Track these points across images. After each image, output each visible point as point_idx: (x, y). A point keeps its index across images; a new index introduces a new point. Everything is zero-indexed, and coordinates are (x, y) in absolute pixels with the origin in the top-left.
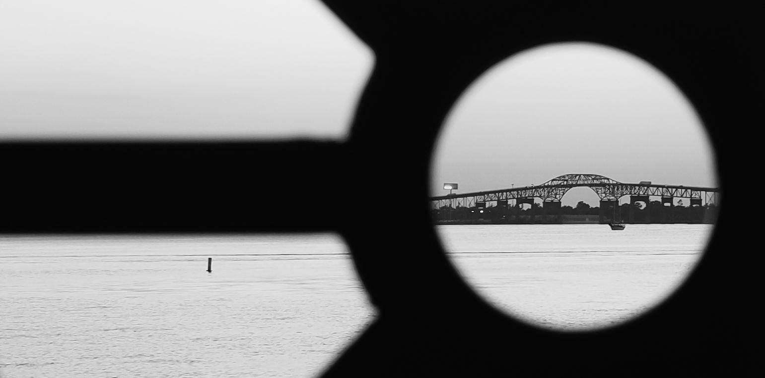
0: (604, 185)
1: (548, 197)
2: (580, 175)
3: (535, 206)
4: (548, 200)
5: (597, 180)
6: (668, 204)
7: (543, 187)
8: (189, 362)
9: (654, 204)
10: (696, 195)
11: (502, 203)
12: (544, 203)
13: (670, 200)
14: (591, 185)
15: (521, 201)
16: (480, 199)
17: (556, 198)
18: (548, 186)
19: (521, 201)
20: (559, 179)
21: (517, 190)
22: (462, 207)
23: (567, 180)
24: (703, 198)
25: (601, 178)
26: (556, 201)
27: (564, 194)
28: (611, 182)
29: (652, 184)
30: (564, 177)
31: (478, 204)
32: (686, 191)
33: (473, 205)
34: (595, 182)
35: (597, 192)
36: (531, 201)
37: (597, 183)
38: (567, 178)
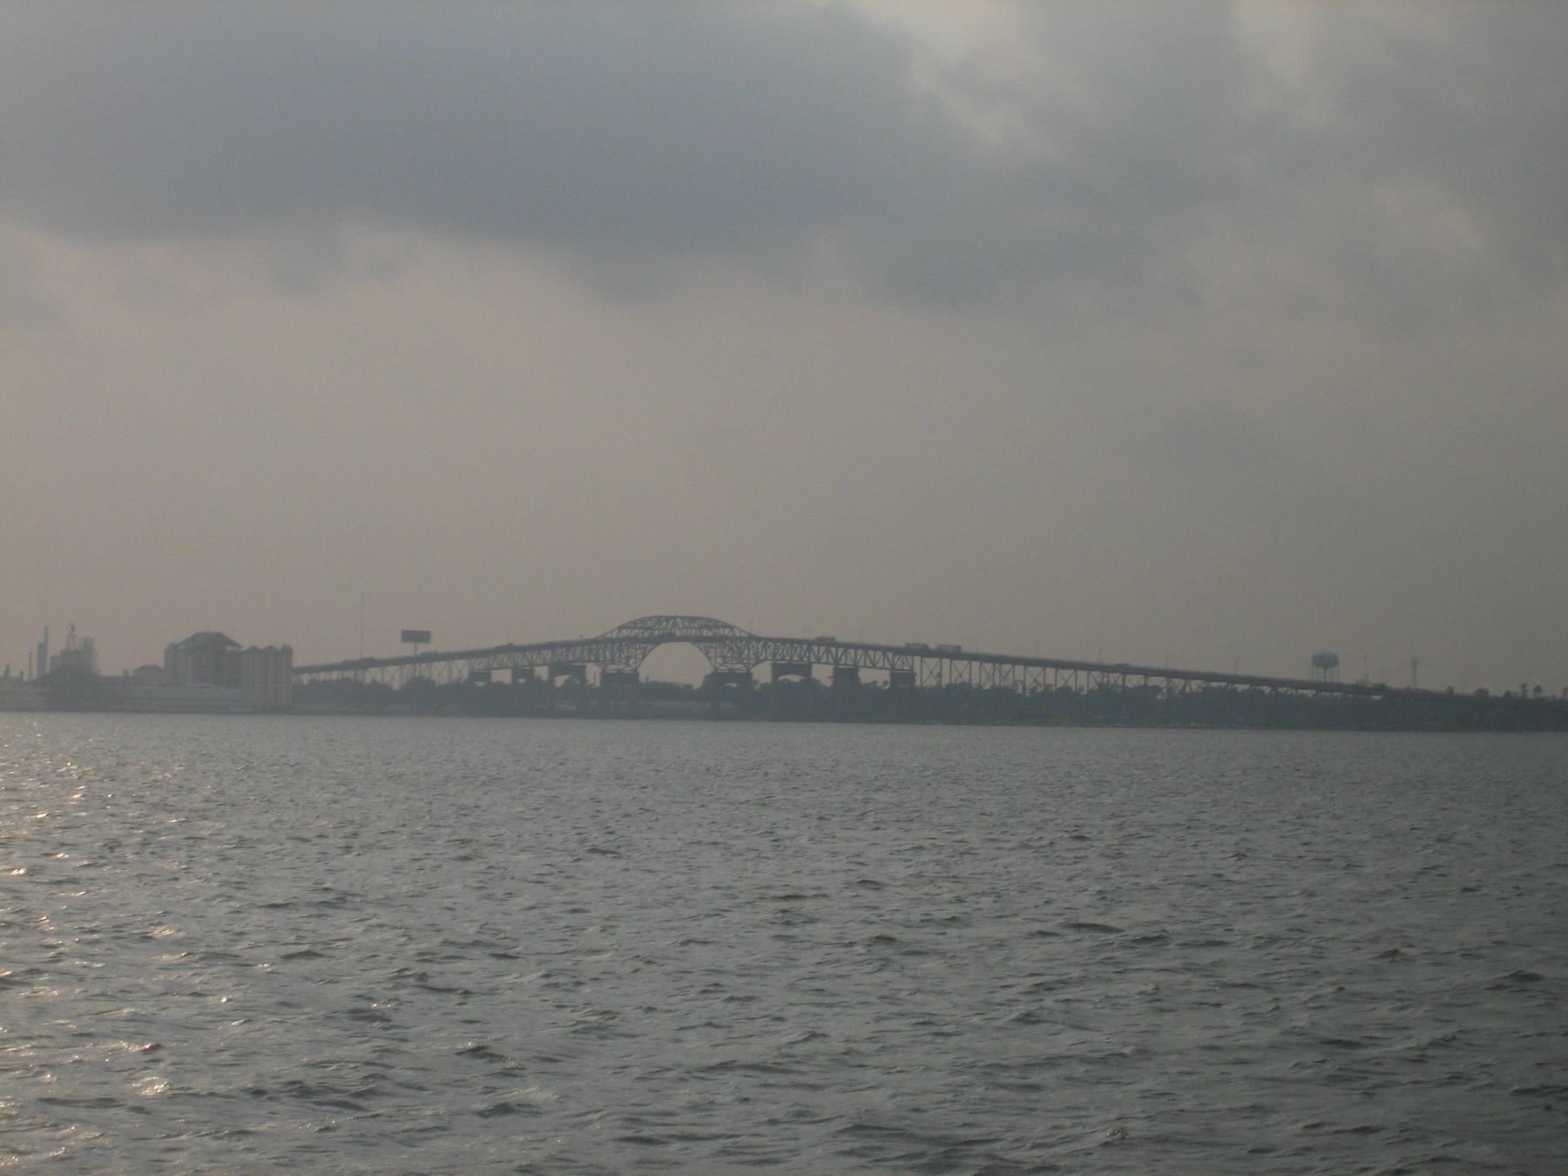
0: (721, 640)
1: (613, 661)
2: (674, 618)
3: (811, 684)
4: (612, 668)
5: (710, 628)
6: (480, 684)
7: (604, 642)
8: (383, 957)
9: (1267, 690)
10: (902, 664)
11: (902, 678)
12: (605, 677)
13: (486, 676)
14: (697, 640)
15: (556, 669)
16: (479, 664)
17: (627, 664)
18: (612, 641)
19: (556, 669)
20: (634, 625)
21: (552, 646)
22: (949, 685)
23: (650, 628)
24: (917, 669)
25: (716, 624)
26: (628, 670)
27: (644, 656)
28: (737, 634)
29: (965, 649)
30: (642, 620)
31: (474, 676)
32: (809, 649)
33: (465, 675)
34: (705, 633)
35: (707, 654)
36: (805, 670)
37: (708, 634)
38: (649, 624)
